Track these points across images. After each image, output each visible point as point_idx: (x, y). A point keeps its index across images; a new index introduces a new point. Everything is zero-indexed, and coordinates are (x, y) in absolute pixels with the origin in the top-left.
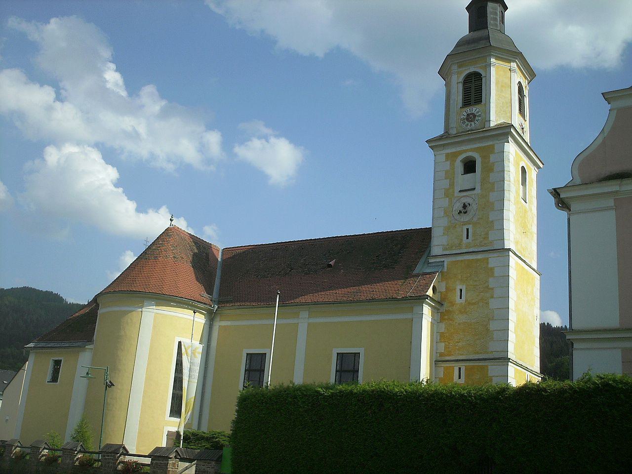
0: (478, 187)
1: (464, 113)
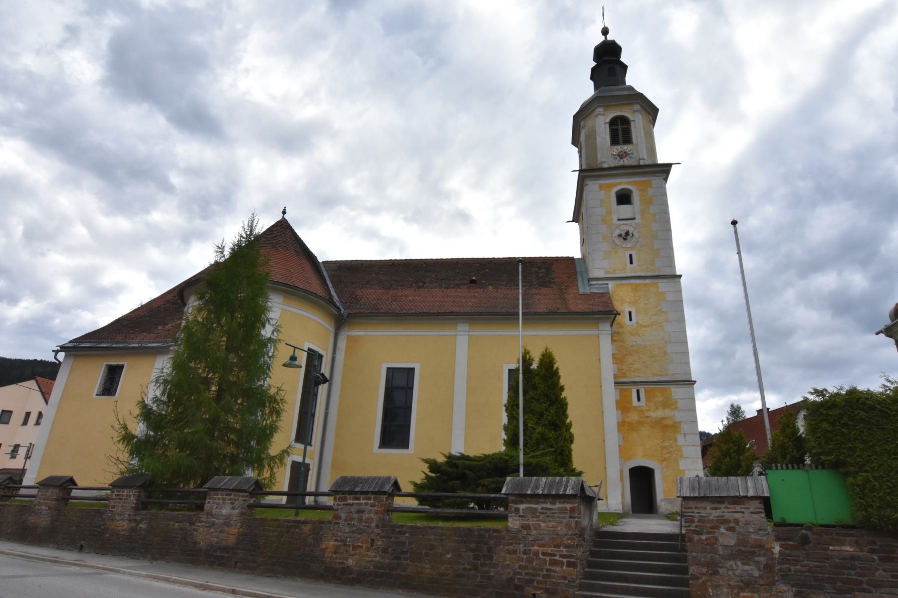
0: (638, 217)
1: (615, 150)
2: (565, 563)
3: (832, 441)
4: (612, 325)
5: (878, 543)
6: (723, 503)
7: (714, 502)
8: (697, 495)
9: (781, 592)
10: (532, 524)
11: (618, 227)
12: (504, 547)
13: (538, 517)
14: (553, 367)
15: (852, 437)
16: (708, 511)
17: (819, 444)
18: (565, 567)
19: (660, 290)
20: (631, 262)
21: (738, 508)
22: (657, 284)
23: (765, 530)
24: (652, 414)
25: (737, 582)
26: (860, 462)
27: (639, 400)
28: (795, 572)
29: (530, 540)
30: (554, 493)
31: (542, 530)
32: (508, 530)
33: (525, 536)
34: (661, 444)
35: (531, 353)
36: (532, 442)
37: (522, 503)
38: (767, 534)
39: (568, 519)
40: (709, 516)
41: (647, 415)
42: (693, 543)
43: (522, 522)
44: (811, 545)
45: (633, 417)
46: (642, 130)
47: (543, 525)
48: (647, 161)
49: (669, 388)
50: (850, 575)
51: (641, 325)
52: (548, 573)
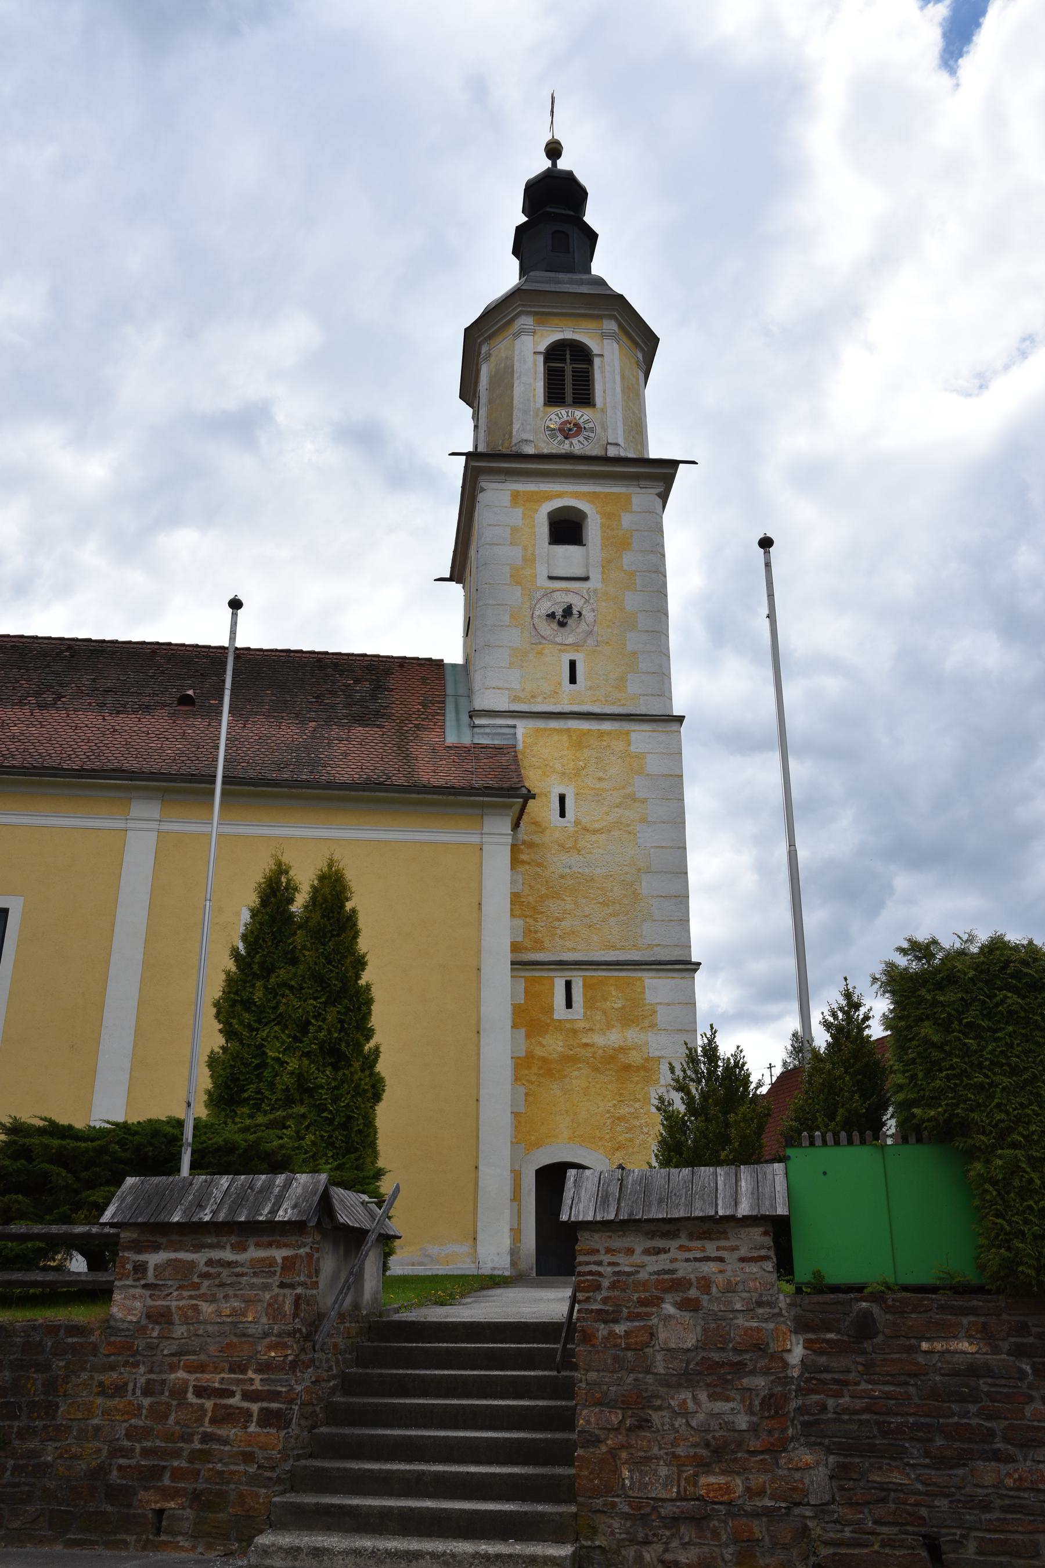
0: (595, 576)
1: (553, 417)
2: (255, 1415)
3: (941, 1071)
4: (516, 826)
5: (1034, 1330)
6: (674, 1235)
7: (651, 1235)
8: (611, 1216)
9: (798, 1469)
10: (178, 1308)
11: (548, 593)
12: (92, 1378)
13: (196, 1286)
14: (343, 906)
15: (986, 1059)
16: (637, 1258)
17: (914, 1077)
18: (253, 1428)
19: (633, 748)
20: (573, 680)
21: (711, 1248)
22: (628, 733)
23: (770, 1304)
24: (598, 1040)
25: (695, 1445)
26: (1002, 1121)
27: (569, 1005)
28: (835, 1413)
29: (165, 1352)
30: (243, 1219)
31: (205, 1322)
32: (109, 1327)
33: (155, 1341)
34: (612, 1110)
35: (291, 873)
36: (274, 1098)
37: (156, 1248)
38: (774, 1315)
39: (277, 1290)
40: (638, 1272)
41: (584, 1040)
42: (593, 1346)
43: (150, 1302)
44: (879, 1339)
45: (554, 1045)
46: (618, 379)
47: (207, 1309)
48: (625, 450)
49: (640, 979)
50: (965, 1414)
51: (585, 829)
52: (205, 1447)
